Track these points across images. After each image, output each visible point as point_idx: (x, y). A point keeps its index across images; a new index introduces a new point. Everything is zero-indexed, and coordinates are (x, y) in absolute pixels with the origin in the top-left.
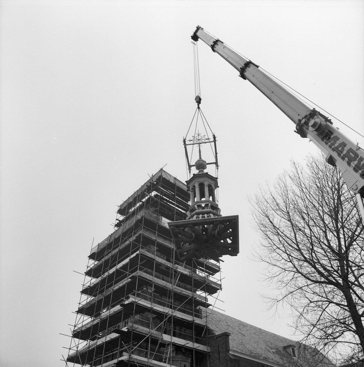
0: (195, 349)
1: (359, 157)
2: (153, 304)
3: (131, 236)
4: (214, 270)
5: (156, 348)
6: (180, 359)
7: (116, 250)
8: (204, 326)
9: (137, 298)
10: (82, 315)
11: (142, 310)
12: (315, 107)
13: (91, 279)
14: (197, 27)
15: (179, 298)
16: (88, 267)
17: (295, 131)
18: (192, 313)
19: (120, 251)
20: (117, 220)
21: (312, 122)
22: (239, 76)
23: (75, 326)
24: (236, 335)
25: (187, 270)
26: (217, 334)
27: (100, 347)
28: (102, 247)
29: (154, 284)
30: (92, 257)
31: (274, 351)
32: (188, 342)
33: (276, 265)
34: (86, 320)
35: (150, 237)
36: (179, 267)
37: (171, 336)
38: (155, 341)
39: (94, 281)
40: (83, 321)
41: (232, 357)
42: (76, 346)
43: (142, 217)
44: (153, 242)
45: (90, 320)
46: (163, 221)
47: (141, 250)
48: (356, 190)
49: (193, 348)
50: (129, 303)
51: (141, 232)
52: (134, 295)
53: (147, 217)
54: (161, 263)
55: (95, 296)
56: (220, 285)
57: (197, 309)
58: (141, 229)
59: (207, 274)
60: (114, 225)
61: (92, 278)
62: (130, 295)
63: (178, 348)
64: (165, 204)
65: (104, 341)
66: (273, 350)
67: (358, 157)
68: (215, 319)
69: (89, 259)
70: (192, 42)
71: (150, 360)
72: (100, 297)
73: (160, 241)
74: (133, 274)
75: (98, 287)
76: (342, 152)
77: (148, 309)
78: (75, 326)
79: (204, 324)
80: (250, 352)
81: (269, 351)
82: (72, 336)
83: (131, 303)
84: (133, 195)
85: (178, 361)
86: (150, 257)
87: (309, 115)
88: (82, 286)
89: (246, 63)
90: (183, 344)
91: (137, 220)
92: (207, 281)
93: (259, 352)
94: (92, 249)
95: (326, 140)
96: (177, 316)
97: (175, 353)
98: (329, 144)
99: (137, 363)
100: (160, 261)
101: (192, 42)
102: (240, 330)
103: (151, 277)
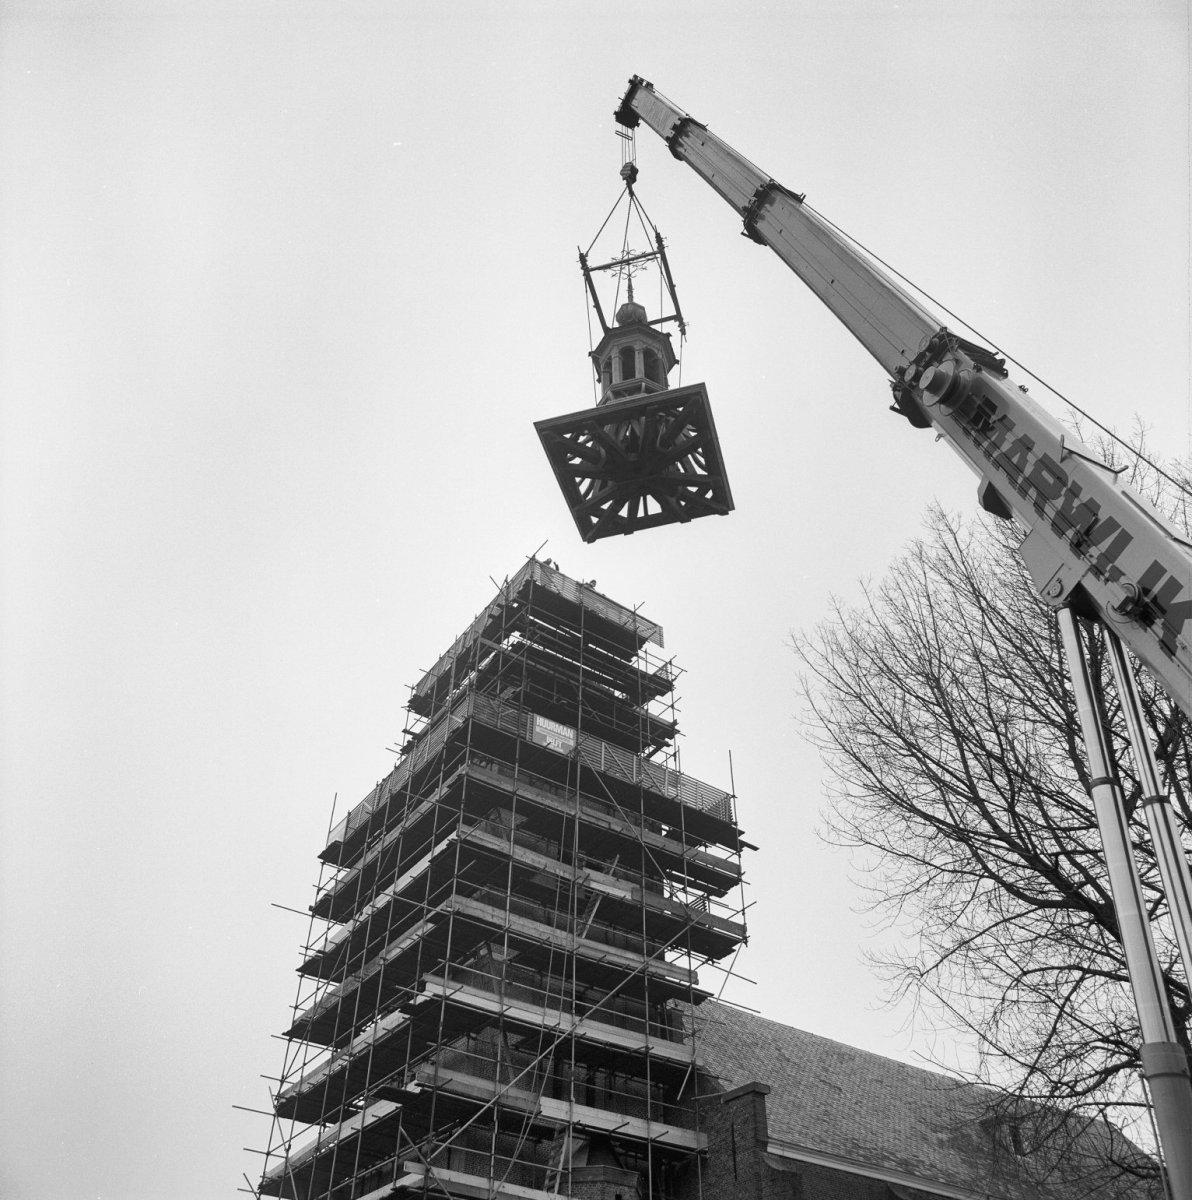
0: (653, 1141)
1: (1069, 484)
2: (506, 1000)
3: (436, 785)
4: (722, 881)
5: (522, 1146)
6: (602, 1178)
7: (395, 833)
8: (687, 1065)
9: (452, 984)
10: (301, 1043)
11: (468, 1021)
13: (329, 929)
14: (630, 81)
15: (596, 975)
16: (319, 890)
17: (892, 408)
18: (644, 1024)
19: (405, 834)
20: (405, 731)
21: (928, 376)
22: (742, 233)
23: (282, 1081)
24: (807, 1091)
25: (623, 883)
26: (730, 1088)
27: (347, 1146)
28: (356, 824)
29: (509, 937)
30: (330, 856)
31: (944, 1136)
32: (628, 1119)
33: (907, 855)
34: (316, 1059)
35: (496, 783)
36: (594, 874)
37: (568, 1104)
38: (512, 1121)
39: (338, 931)
40: (305, 1064)
41: (774, 1165)
42: (284, 1144)
43: (466, 720)
44: (504, 800)
45: (327, 1055)
46: (538, 729)
47: (463, 827)
48: (1057, 596)
49: (646, 1139)
50: (426, 1001)
51: (462, 770)
52: (440, 974)
53: (484, 717)
54: (535, 868)
55: (338, 980)
56: (743, 929)
57: (668, 1008)
58: (462, 761)
59: (700, 893)
60: (398, 749)
61: (331, 924)
62: (427, 977)
63: (598, 1143)
64: (552, 672)
65: (360, 1128)
66: (940, 1135)
67: (1065, 485)
68: (737, 1040)
69: (323, 864)
70: (617, 133)
71: (497, 1183)
72: (353, 984)
73: (529, 794)
74: (438, 909)
75: (346, 952)
76: (1019, 469)
77: (491, 1017)
78: (282, 1081)
79: (686, 1058)
80: (849, 1145)
81: (925, 1139)
82: (273, 1111)
83: (432, 1000)
84: (452, 648)
85: (596, 1182)
86: (496, 847)
87: (929, 349)
88: (303, 951)
89: (761, 189)
90: (611, 1129)
91: (454, 732)
92: (693, 917)
93: (886, 1144)
94: (330, 832)
95: (977, 431)
96: (589, 1034)
97: (586, 1157)
98: (986, 444)
100: (529, 861)
101: (617, 133)
102: (827, 1070)
103: (498, 912)
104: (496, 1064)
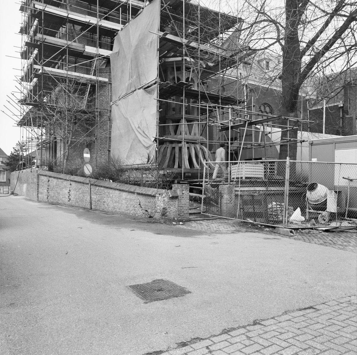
12: (211, 237)
99: (52, 75)
104: (66, 34)
